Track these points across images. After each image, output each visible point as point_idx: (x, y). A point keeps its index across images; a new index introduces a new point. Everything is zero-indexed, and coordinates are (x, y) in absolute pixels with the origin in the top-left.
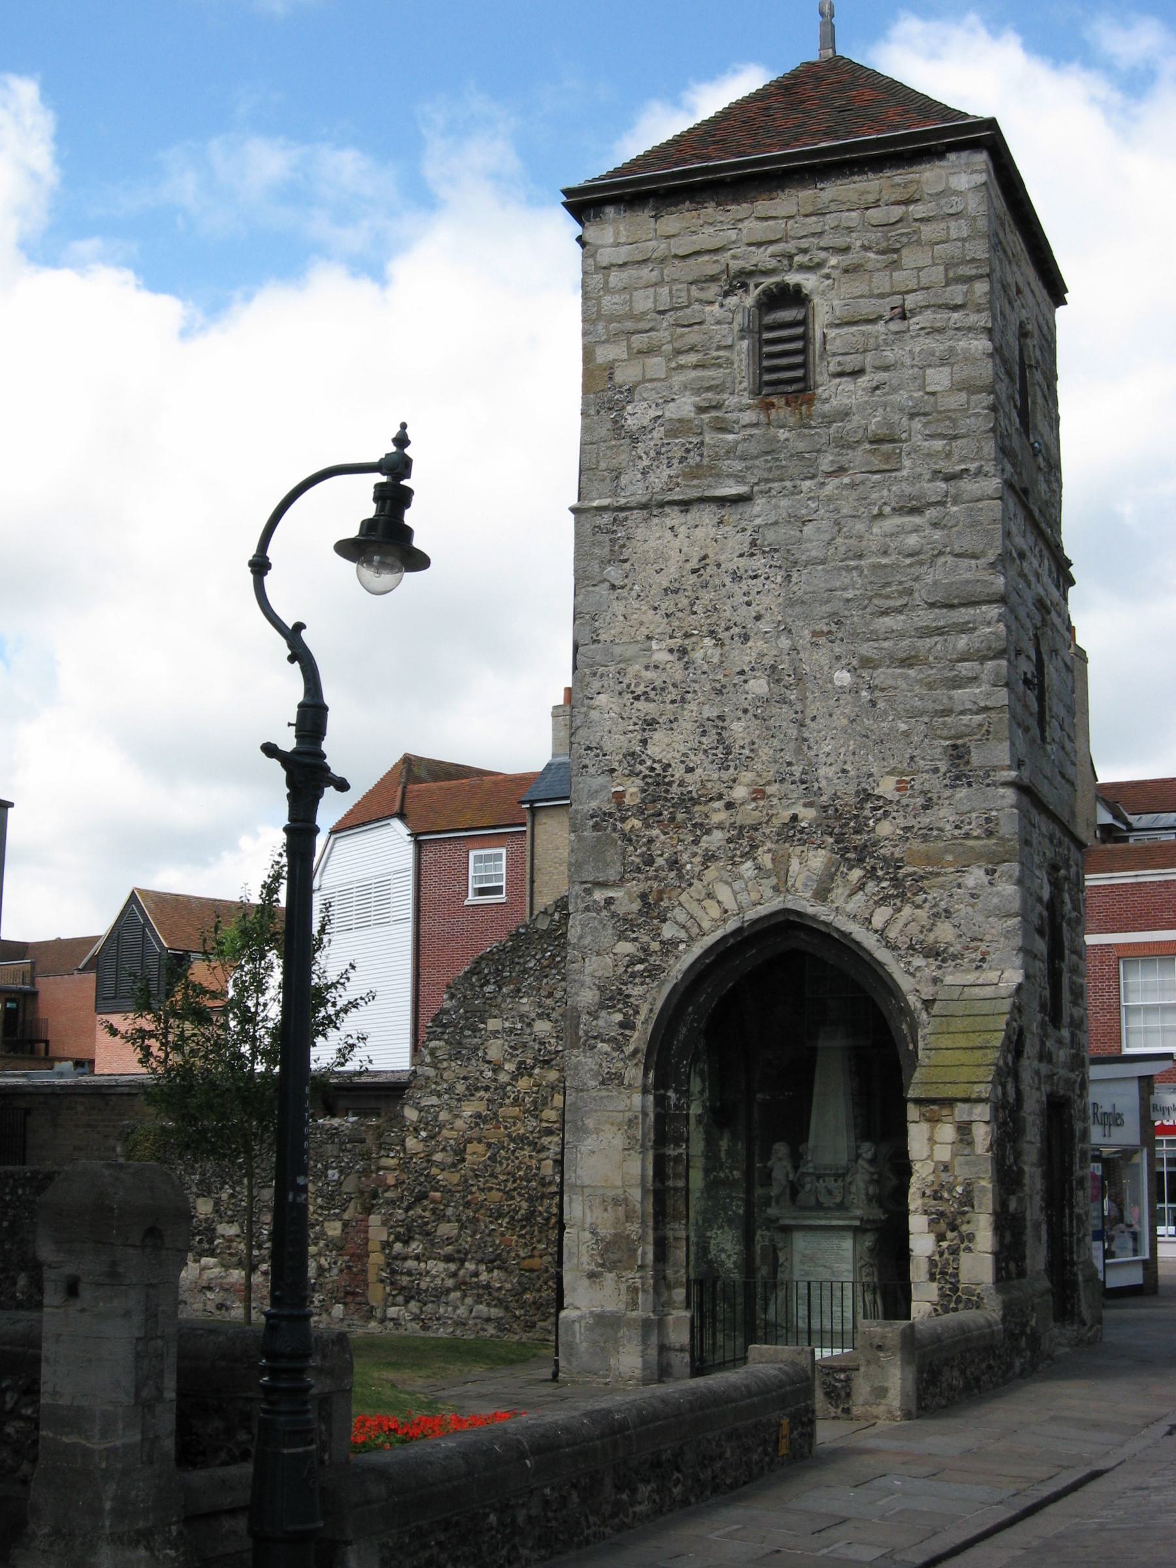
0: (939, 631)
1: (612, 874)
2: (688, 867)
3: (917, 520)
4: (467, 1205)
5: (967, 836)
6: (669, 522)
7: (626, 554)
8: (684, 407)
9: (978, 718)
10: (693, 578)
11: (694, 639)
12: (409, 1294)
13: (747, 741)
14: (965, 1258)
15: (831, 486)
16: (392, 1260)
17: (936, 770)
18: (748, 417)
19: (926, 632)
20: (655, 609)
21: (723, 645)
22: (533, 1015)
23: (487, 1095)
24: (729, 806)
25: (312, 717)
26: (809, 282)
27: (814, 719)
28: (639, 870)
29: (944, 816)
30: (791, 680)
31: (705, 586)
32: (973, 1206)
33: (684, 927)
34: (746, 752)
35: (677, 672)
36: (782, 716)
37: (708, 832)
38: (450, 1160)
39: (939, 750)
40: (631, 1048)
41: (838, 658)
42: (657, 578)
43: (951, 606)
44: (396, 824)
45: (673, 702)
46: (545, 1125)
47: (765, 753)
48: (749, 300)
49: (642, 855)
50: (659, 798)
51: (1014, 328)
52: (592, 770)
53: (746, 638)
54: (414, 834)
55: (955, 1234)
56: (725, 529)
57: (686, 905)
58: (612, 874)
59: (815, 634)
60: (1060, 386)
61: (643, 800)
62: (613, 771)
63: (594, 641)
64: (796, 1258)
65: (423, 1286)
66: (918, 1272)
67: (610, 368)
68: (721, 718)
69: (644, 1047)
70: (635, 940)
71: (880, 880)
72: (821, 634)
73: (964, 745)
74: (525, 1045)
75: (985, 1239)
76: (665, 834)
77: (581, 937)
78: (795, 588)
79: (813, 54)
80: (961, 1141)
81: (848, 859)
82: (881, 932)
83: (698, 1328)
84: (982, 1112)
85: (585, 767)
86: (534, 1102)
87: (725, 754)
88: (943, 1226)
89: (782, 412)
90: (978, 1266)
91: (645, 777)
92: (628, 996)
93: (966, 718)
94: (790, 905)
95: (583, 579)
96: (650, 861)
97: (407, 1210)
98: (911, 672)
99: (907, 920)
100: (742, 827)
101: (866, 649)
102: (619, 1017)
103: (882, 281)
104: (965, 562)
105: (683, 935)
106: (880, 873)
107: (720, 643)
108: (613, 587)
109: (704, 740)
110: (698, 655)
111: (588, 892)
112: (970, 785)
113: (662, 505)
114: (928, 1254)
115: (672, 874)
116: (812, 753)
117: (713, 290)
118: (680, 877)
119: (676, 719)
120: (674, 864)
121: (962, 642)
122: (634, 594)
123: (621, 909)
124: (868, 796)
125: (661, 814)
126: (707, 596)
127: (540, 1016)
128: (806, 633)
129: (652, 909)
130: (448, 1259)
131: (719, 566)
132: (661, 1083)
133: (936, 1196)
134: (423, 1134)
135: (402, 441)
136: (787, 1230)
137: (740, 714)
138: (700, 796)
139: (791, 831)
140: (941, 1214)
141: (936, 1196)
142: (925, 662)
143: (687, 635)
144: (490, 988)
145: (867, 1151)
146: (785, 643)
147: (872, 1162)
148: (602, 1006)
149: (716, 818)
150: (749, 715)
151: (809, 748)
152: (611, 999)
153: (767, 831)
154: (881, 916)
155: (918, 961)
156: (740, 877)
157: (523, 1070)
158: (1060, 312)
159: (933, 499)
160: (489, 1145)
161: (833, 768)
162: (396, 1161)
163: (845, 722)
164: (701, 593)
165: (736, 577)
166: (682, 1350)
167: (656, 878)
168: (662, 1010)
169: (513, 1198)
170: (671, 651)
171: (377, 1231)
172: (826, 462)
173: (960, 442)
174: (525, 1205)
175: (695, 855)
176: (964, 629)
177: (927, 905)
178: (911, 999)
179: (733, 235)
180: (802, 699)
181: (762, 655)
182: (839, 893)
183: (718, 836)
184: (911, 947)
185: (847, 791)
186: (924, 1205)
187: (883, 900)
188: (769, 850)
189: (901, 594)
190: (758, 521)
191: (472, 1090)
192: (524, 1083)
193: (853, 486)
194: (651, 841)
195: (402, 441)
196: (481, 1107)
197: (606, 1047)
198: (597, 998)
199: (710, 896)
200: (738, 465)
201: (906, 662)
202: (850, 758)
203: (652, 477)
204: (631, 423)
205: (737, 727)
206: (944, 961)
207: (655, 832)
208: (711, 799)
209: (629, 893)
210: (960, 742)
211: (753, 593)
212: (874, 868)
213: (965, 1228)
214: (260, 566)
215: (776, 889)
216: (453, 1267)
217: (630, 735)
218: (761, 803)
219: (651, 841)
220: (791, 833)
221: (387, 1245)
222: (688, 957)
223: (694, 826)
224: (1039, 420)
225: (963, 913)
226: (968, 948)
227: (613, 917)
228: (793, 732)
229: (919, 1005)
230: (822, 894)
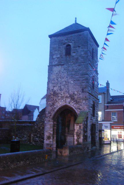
8: (59, 56)
14: (80, 140)
16: (33, 139)
24: (61, 94)
26: (71, 44)
29: (81, 96)
35: (57, 81)
36: (66, 86)
48: (65, 46)
75: (82, 138)
79: (74, 23)
83: (57, 146)
87: (61, 90)
101: (74, 79)
120: (56, 100)
121: (83, 78)
129: (53, 104)
132: (54, 121)
133: (77, 133)
136: (67, 136)
139: (67, 97)
146: (67, 79)
154: (75, 105)
155: (78, 110)
156: (62, 101)
165: (63, 72)
171: (32, 135)
176: (84, 77)
182: (71, 103)
185: (72, 93)
187: (75, 104)
196: (42, 124)
205: (62, 87)
222: (56, 110)
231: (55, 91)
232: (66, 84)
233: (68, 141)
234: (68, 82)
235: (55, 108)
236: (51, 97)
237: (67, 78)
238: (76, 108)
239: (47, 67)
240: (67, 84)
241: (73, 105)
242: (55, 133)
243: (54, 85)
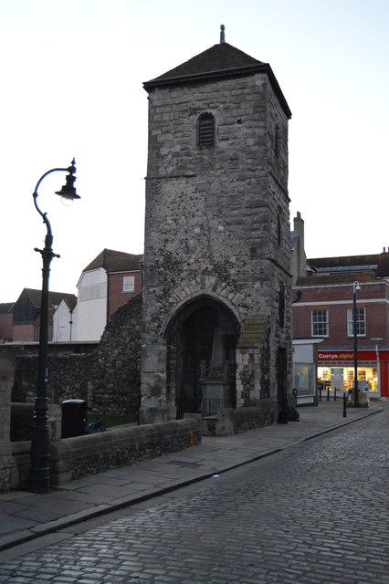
3: (243, 183)
8: (177, 148)
9: (258, 240)
12: (101, 404)
15: (219, 172)
18: (197, 152)
24: (189, 264)
25: (49, 239)
26: (214, 112)
29: (248, 268)
47: (199, 249)
51: (274, 126)
60: (289, 143)
66: (239, 395)
67: (156, 137)
75: (258, 387)
84: (257, 351)
87: (188, 250)
89: (206, 151)
90: (256, 394)
99: (239, 297)
101: (227, 220)
103: (235, 113)
107: (186, 218)
117: (187, 114)
120: (173, 281)
121: (255, 218)
129: (166, 293)
132: (169, 343)
135: (73, 162)
139: (206, 272)
149: (185, 268)
154: (231, 296)
155: (241, 309)
158: (289, 121)
165: (191, 199)
171: (90, 387)
172: (217, 166)
178: (240, 320)
179: (192, 97)
180: (210, 234)
182: (219, 290)
185: (222, 261)
195: (73, 162)
200: (192, 166)
201: (239, 224)
204: (162, 153)
205: (191, 242)
214: (35, 195)
222: (174, 310)
224: (282, 155)
230: (214, 289)
241: (223, 295)
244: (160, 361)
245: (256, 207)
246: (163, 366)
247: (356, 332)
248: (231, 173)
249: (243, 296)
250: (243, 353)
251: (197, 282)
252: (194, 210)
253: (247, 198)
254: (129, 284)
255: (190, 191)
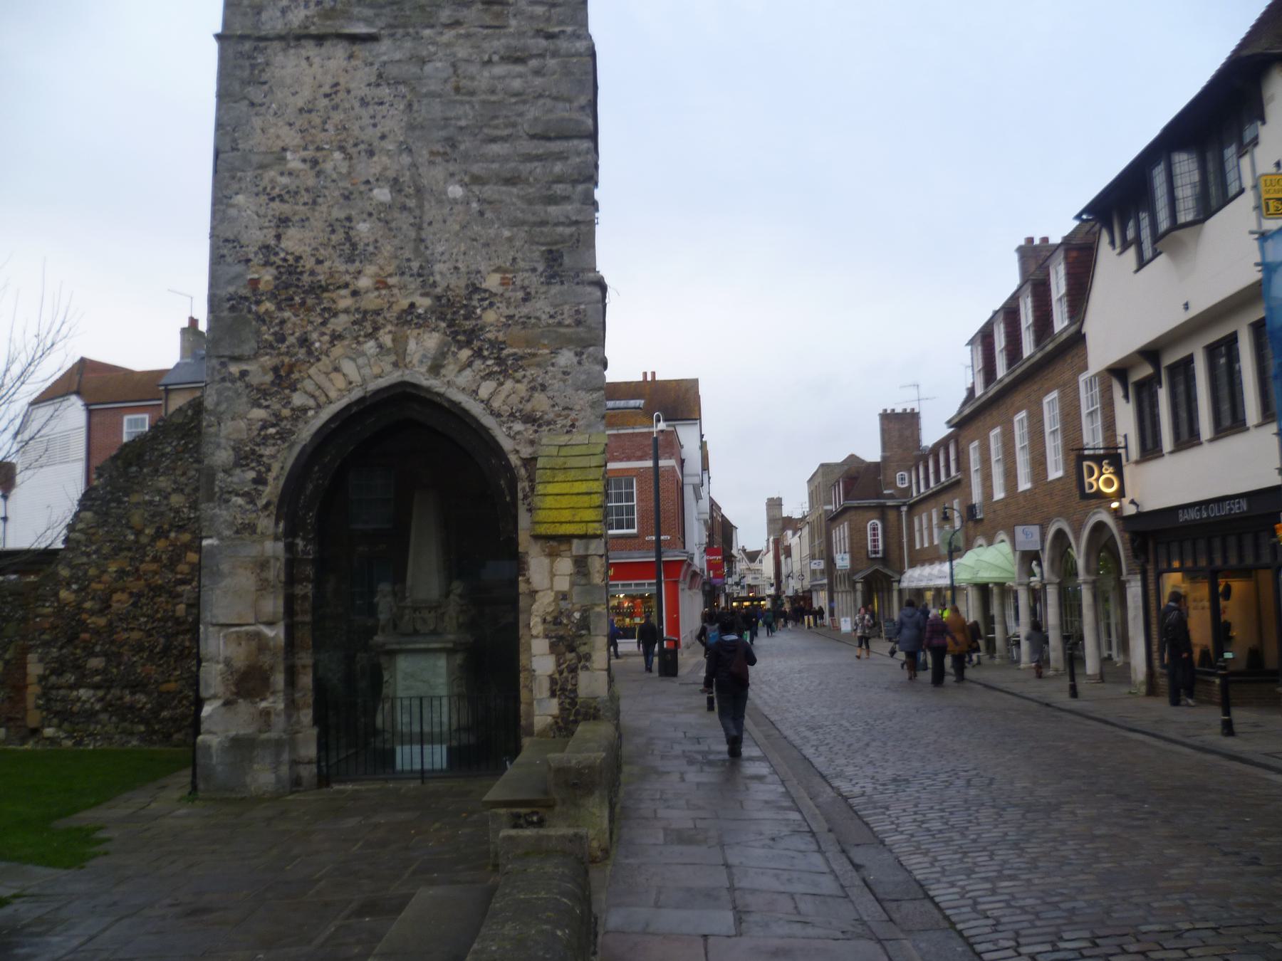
0: (538, 158)
1: (247, 349)
2: (317, 345)
3: (519, 68)
4: (112, 642)
5: (560, 324)
6: (304, 53)
7: (265, 77)
9: (568, 231)
10: (325, 102)
11: (324, 153)
13: (372, 239)
14: (583, 676)
15: (449, 35)
16: (45, 694)
17: (534, 270)
19: (529, 158)
20: (290, 125)
21: (351, 158)
22: (169, 490)
23: (130, 554)
24: (355, 293)
27: (430, 224)
28: (272, 347)
29: (541, 307)
30: (411, 191)
31: (335, 108)
32: (589, 629)
33: (313, 396)
34: (371, 249)
36: (403, 221)
37: (335, 315)
38: (97, 607)
39: (537, 253)
40: (264, 502)
41: (452, 175)
42: (291, 100)
43: (549, 139)
44: (74, 398)
45: (305, 204)
46: (179, 576)
47: (387, 249)
49: (275, 334)
50: (291, 285)
52: (229, 259)
53: (371, 153)
54: (87, 405)
55: (573, 655)
56: (354, 63)
57: (315, 377)
58: (247, 349)
59: (432, 153)
61: (276, 287)
62: (248, 261)
63: (233, 149)
64: (399, 676)
65: (75, 709)
68: (349, 219)
69: (276, 500)
70: (267, 407)
71: (485, 358)
72: (438, 153)
73: (558, 251)
74: (162, 514)
76: (296, 316)
77: (218, 404)
78: (416, 115)
80: (578, 573)
81: (458, 341)
82: (487, 403)
83: (323, 745)
85: (223, 256)
86: (170, 559)
87: (353, 251)
88: (562, 647)
91: (278, 267)
92: (261, 456)
93: (560, 229)
94: (407, 378)
95: (223, 95)
96: (282, 339)
97: (61, 648)
98: (515, 190)
99: (508, 393)
100: (366, 312)
101: (476, 169)
102: (252, 475)
104: (560, 105)
105: (312, 403)
106: (486, 353)
107: (349, 157)
108: (252, 104)
109: (333, 237)
110: (328, 166)
111: (223, 365)
112: (562, 283)
113: (299, 38)
114: (550, 672)
115: (303, 351)
116: (428, 252)
118: (310, 353)
119: (308, 219)
120: (304, 341)
121: (558, 168)
122: (271, 111)
123: (255, 379)
124: (476, 289)
125: (292, 299)
126: (337, 117)
127: (174, 490)
128: (425, 152)
129: (284, 379)
130: (96, 687)
131: (349, 92)
132: (290, 533)
134: (74, 587)
136: (392, 654)
137: (365, 216)
138: (328, 285)
139: (408, 317)
140: (561, 638)
141: (556, 622)
142: (526, 181)
143: (319, 149)
144: (134, 469)
145: (457, 587)
146: (405, 159)
147: (460, 596)
148: (237, 464)
150: (374, 217)
151: (427, 248)
152: (246, 458)
153: (388, 315)
154: (486, 389)
155: (518, 426)
156: (363, 354)
157: (160, 534)
159: (535, 52)
160: (131, 594)
161: (447, 265)
162: (50, 610)
163: (457, 227)
164: (333, 114)
165: (364, 102)
166: (309, 763)
167: (287, 353)
168: (294, 466)
169: (151, 635)
170: (304, 161)
171: (35, 669)
172: (445, 15)
173: (558, 10)
174: (162, 640)
175: (323, 334)
176: (561, 156)
177: (526, 381)
178: (514, 459)
180: (421, 207)
181: (385, 169)
182: (450, 370)
183: (343, 318)
184: (512, 415)
186: (545, 630)
187: (489, 376)
188: (390, 332)
189: (506, 126)
190: (385, 58)
191: (117, 551)
192: (161, 544)
193: (468, 36)
194: (283, 322)
197: (240, 501)
198: (232, 458)
199: (337, 369)
201: (511, 181)
202: (461, 257)
203: (290, 16)
206: (540, 426)
207: (287, 314)
208: (339, 287)
209: (263, 367)
210: (554, 248)
211: (379, 117)
212: (480, 349)
213: (583, 649)
215: (395, 365)
216: (100, 693)
217: (265, 231)
218: (384, 292)
219: (283, 322)
220: (409, 318)
221: (42, 678)
222: (306, 433)
223: (324, 309)
225: (556, 386)
226: (560, 415)
227: (247, 387)
228: (413, 234)
229: (519, 463)
230: (435, 369)
231: (298, 259)
232: (404, 208)
233: (400, 694)
234: (419, 191)
235: (304, 410)
236: (261, 319)
237: (409, 150)
238: (499, 415)
239: (212, 50)
240: (411, 203)
241: (464, 385)
242: (304, 635)
243: (286, 209)
244: (263, 586)
245: (558, 138)
246: (273, 605)
247: (630, 526)
248: (485, 37)
249: (522, 388)
250: (553, 555)
251: (380, 346)
252: (371, 134)
253: (532, 112)
254: (134, 425)
255: (359, 81)
